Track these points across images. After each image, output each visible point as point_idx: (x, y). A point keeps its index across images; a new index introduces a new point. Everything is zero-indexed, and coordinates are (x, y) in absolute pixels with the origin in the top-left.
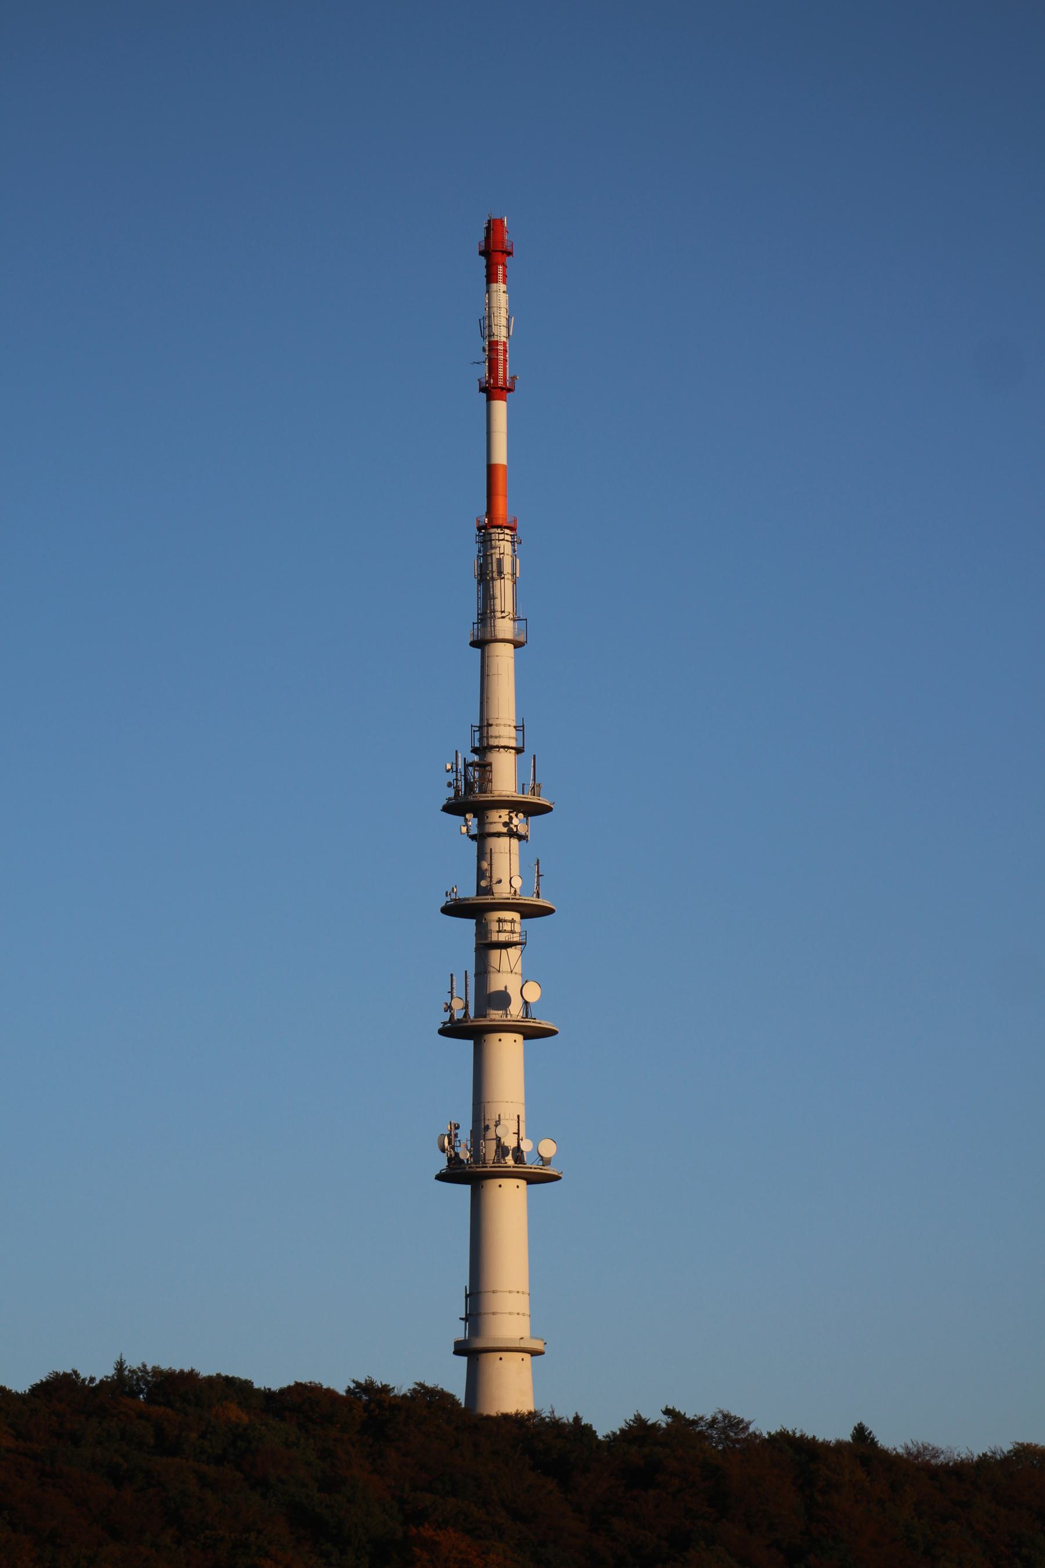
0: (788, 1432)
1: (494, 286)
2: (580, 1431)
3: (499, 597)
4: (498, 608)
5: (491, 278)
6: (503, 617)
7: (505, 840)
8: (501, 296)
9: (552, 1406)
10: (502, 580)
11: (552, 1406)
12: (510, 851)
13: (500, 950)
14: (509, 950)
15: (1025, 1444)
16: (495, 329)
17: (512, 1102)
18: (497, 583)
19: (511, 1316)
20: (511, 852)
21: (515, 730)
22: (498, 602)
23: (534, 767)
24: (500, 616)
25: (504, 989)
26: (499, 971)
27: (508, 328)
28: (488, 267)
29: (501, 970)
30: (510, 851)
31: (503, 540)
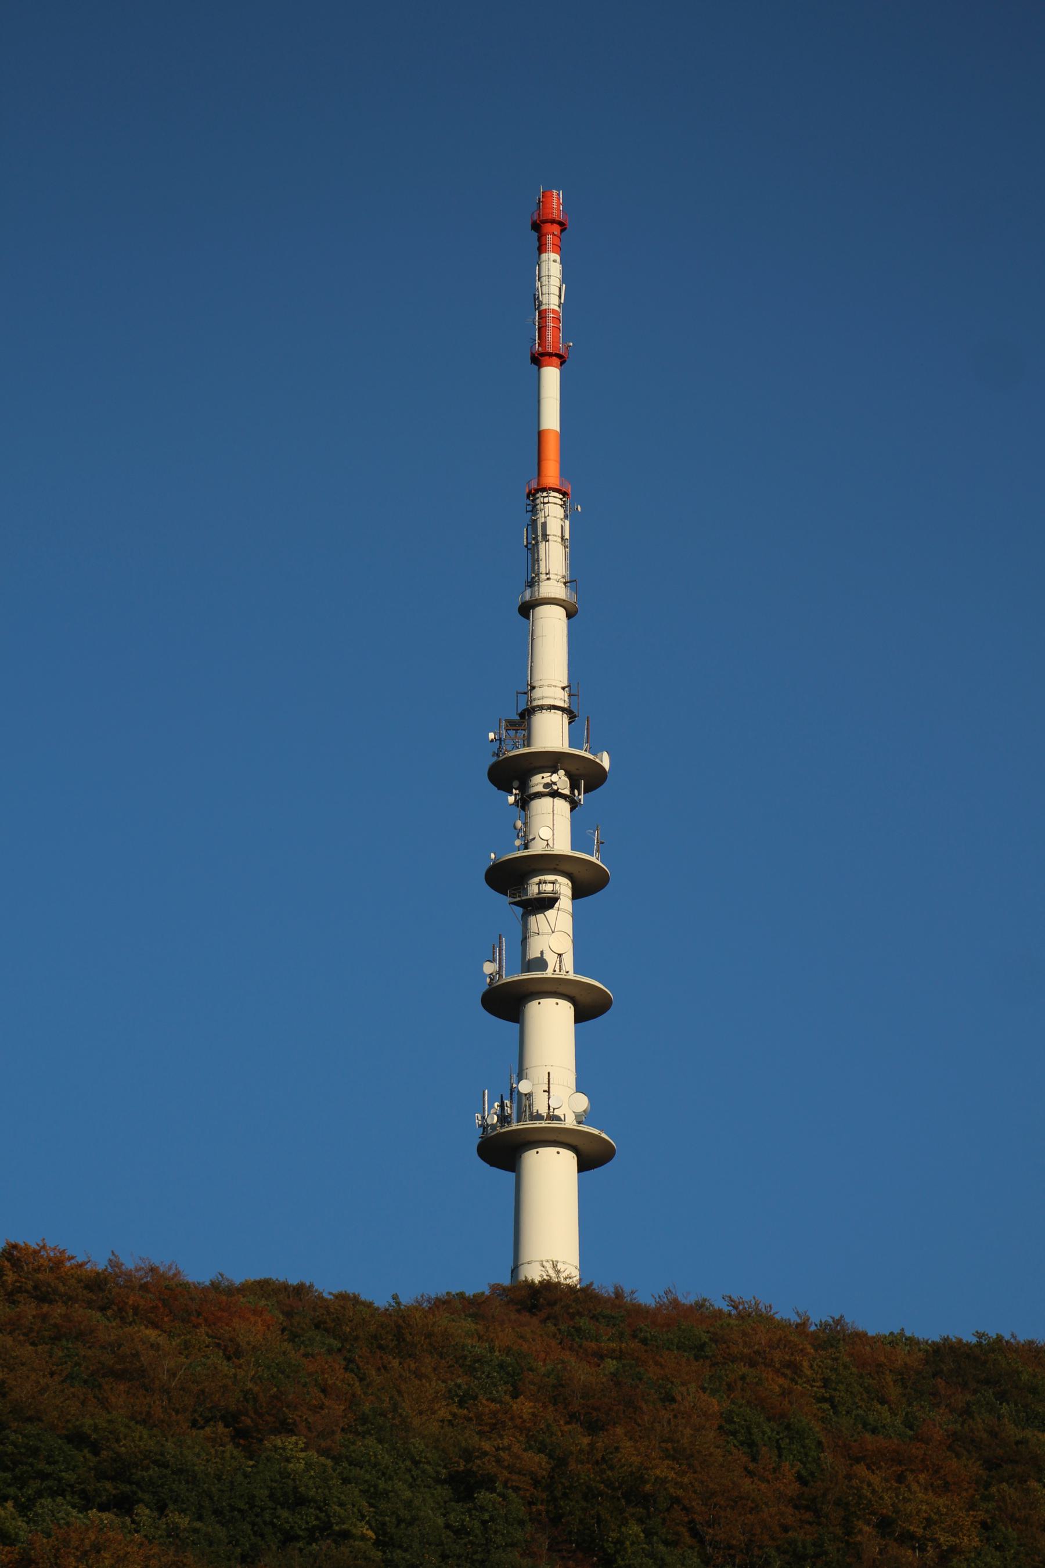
0: (412, 1304)
1: (544, 256)
2: (866, 1334)
3: (544, 560)
4: (543, 570)
5: (541, 249)
6: (548, 579)
7: (547, 801)
8: (552, 265)
9: (637, 1291)
10: (547, 543)
11: (637, 1291)
12: (553, 811)
13: (534, 916)
14: (556, 800)
15: (472, 1297)
16: (544, 299)
17: (560, 619)
18: (542, 546)
19: (556, 534)
20: (555, 812)
21: (564, 586)
22: (542, 564)
23: (588, 729)
24: (546, 578)
25: (540, 956)
26: (538, 934)
27: (560, 297)
28: (539, 239)
29: (541, 931)
30: (553, 811)
31: (548, 503)
